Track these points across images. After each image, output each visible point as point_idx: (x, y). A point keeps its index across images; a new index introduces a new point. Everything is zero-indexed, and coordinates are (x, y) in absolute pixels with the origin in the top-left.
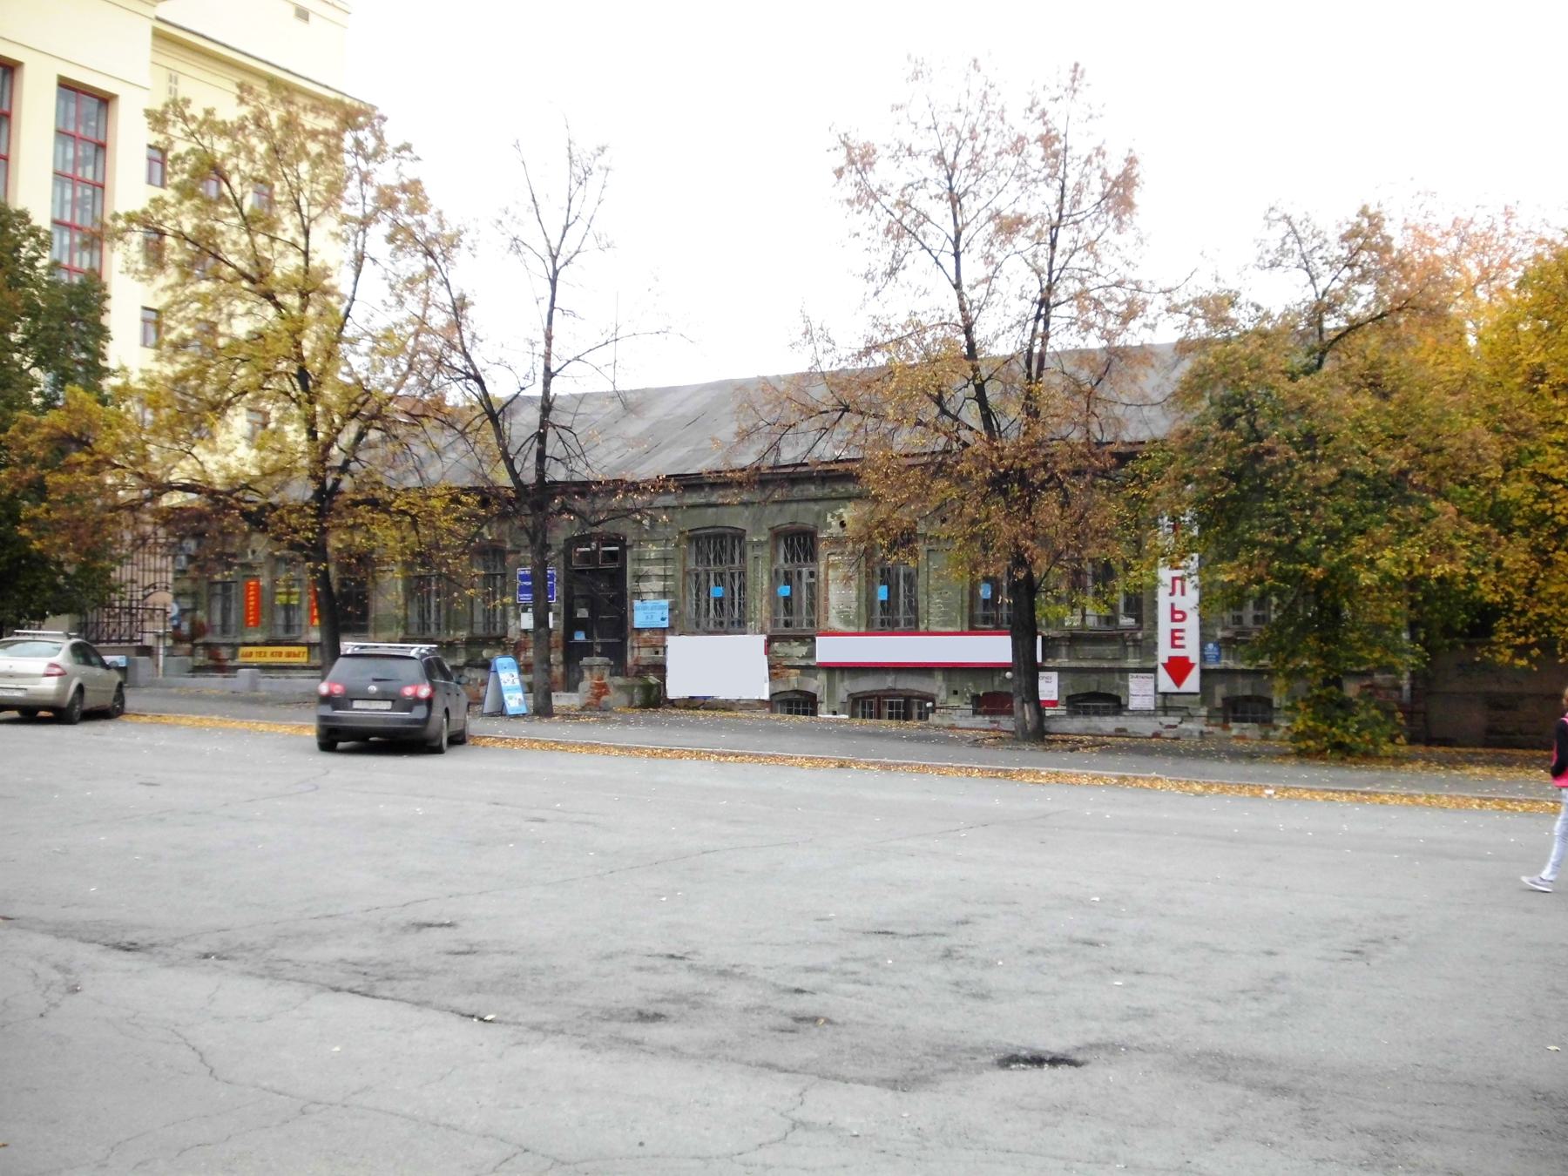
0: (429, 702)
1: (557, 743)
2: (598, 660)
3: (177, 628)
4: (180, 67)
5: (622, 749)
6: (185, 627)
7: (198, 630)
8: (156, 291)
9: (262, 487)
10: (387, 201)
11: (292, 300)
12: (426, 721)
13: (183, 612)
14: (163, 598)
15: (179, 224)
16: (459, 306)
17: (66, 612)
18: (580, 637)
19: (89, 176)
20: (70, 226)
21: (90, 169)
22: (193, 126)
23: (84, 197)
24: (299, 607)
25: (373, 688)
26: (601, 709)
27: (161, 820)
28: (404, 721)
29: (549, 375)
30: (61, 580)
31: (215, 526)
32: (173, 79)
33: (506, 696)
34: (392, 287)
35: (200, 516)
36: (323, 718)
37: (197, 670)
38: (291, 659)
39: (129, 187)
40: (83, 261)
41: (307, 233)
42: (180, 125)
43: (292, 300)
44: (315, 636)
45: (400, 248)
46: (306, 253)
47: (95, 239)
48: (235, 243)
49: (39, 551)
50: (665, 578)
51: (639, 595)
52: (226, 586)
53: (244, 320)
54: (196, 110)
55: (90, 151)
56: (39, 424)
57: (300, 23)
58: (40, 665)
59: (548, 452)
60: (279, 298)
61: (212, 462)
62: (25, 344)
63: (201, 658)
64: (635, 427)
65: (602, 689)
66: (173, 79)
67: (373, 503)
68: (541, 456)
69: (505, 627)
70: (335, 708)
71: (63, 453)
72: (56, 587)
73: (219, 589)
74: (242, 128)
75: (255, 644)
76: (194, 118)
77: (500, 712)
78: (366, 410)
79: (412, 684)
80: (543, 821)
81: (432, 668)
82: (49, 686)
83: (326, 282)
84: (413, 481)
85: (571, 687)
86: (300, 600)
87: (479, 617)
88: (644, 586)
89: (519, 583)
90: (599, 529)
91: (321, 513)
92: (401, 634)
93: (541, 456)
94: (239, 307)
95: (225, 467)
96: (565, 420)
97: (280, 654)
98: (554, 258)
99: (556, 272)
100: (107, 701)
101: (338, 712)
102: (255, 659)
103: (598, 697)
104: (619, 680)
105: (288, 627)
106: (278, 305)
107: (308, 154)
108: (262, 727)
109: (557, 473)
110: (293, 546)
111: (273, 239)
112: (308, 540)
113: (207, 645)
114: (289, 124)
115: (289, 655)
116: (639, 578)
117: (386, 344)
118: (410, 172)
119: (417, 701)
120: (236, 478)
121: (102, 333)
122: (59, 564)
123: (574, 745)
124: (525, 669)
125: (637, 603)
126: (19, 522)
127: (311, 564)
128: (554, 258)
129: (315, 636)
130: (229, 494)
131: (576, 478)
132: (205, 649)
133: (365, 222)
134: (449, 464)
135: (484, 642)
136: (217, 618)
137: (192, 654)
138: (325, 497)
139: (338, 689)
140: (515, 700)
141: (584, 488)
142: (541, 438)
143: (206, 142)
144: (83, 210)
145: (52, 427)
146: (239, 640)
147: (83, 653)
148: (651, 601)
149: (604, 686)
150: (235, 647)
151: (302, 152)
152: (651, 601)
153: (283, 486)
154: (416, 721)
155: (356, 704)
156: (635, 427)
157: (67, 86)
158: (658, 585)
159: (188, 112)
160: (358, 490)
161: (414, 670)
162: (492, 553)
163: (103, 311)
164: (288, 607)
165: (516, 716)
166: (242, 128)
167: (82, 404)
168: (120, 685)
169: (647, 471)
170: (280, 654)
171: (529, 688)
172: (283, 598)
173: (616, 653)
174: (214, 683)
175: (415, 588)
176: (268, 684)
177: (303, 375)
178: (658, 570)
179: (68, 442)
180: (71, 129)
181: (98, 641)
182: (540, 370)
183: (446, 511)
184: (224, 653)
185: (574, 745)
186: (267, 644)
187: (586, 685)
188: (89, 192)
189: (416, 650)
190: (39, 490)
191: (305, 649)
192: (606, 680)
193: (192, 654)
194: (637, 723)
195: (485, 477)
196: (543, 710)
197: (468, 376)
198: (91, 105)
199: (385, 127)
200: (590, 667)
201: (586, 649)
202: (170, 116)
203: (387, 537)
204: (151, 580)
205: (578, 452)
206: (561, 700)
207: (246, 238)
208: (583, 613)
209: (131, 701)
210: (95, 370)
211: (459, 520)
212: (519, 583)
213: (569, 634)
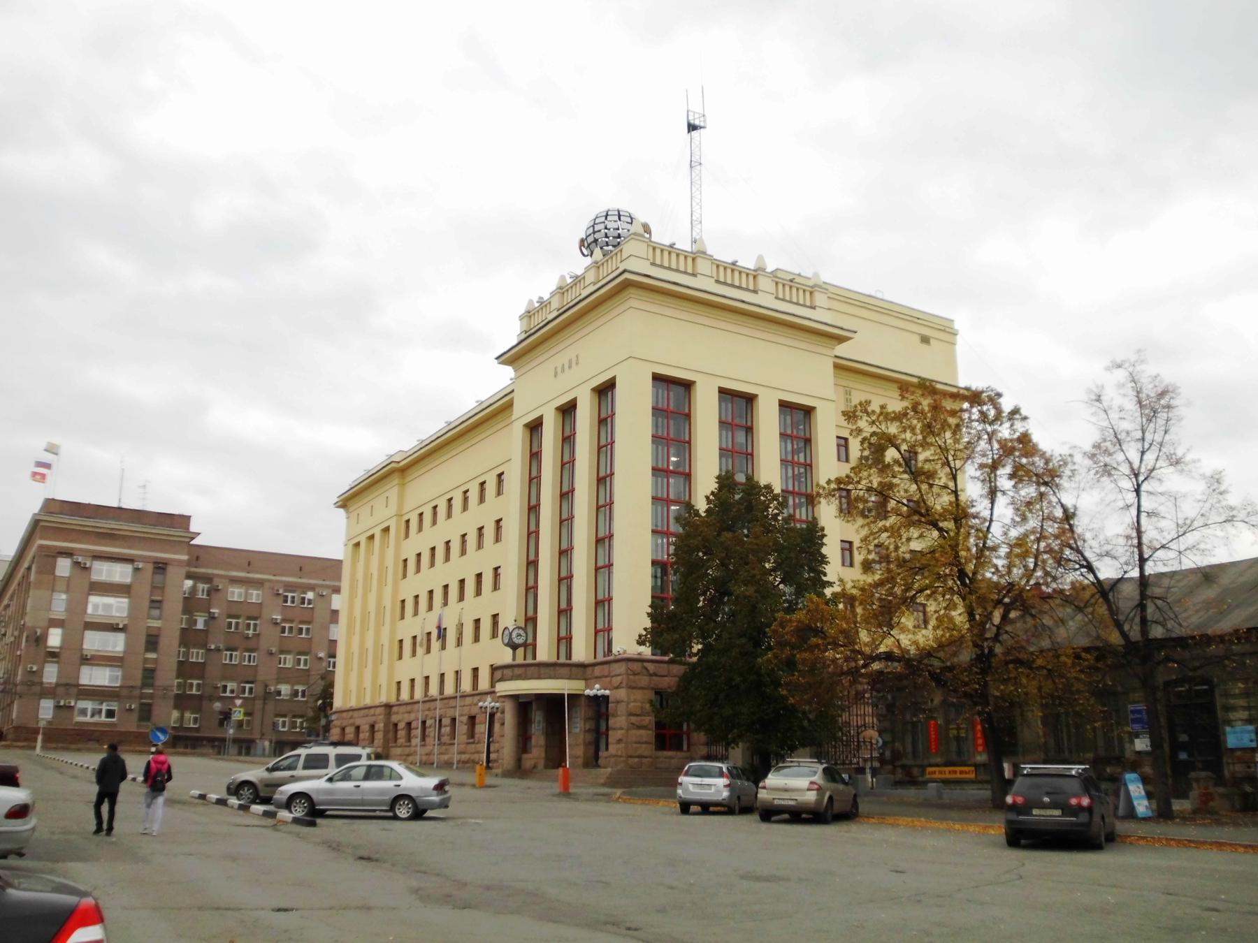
0: (1089, 809)
1: (1190, 841)
2: (1203, 774)
3: (882, 754)
4: (851, 384)
5: (1246, 847)
6: (888, 754)
7: (896, 756)
8: (854, 531)
9: (941, 654)
10: (1007, 449)
11: (948, 525)
12: (1088, 825)
13: (885, 743)
14: (872, 734)
15: (871, 482)
16: (1068, 516)
17: (810, 745)
18: (1183, 756)
19: (802, 460)
20: (793, 493)
21: (802, 455)
22: (874, 418)
23: (800, 473)
24: (967, 738)
25: (1046, 799)
26: (1209, 813)
27: (919, 901)
28: (1072, 823)
29: (1142, 561)
30: (805, 723)
31: (906, 681)
32: (848, 393)
33: (1135, 803)
34: (1018, 509)
35: (899, 677)
36: (1009, 823)
37: (898, 784)
38: (963, 776)
39: (828, 467)
40: (802, 514)
41: (954, 478)
42: (865, 418)
43: (948, 525)
44: (981, 758)
45: (1021, 481)
46: (955, 492)
47: (811, 500)
48: (906, 491)
49: (793, 705)
50: (1248, 708)
51: (1229, 722)
52: (914, 725)
53: (919, 541)
54: (875, 406)
55: (802, 444)
56: (790, 620)
57: (924, 346)
58: (803, 783)
59: (1149, 618)
60: (941, 525)
61: (905, 640)
62: (774, 569)
63: (899, 775)
64: (1210, 593)
65: (1207, 798)
66: (848, 393)
67: (1019, 662)
68: (1144, 621)
69: (1122, 750)
70: (1020, 813)
71: (805, 640)
72: (803, 728)
73: (909, 727)
74: (905, 414)
75: (937, 765)
76: (873, 412)
77: (1131, 814)
78: (1019, 599)
79: (1075, 796)
80: (1217, 910)
81: (1088, 784)
82: (811, 797)
83: (973, 510)
84: (1046, 644)
85: (1183, 795)
86: (967, 733)
87: (1101, 743)
88: (1232, 716)
89: (1131, 716)
90: (1199, 672)
91: (984, 672)
92: (1042, 756)
93: (1144, 621)
94: (914, 532)
95: (915, 643)
96: (1157, 591)
97: (955, 772)
98: (1136, 476)
99: (1139, 486)
100: (848, 807)
101: (1021, 817)
102: (937, 776)
103: (1206, 802)
104: (1221, 790)
105: (959, 753)
106: (940, 530)
107: (950, 426)
108: (957, 826)
109: (1157, 632)
110: (966, 695)
111: (931, 486)
112: (976, 690)
113: (903, 767)
114: (935, 408)
115: (961, 772)
116: (1228, 709)
117: (1019, 547)
118: (1020, 427)
119: (1080, 808)
120: (924, 649)
121: (823, 560)
122: (804, 713)
123: (1204, 843)
124: (1145, 780)
125: (1228, 729)
126: (779, 685)
127: (979, 708)
128: (1136, 476)
129: (981, 758)
130: (920, 662)
131: (1174, 635)
132: (902, 770)
133: (994, 466)
134: (1071, 630)
135: (1108, 761)
136: (909, 748)
137: (893, 772)
138: (984, 660)
139: (1020, 800)
140: (1142, 807)
141: (1181, 642)
142: (1142, 606)
143: (883, 427)
144: (800, 482)
145: (799, 621)
146: (926, 762)
147: (830, 774)
148: (1239, 727)
149: (1211, 794)
150: (923, 768)
151: (945, 426)
152: (1239, 727)
153: (955, 654)
154: (1082, 824)
155: (1035, 812)
156: (1210, 593)
157: (784, 406)
158: (1244, 714)
159: (870, 409)
160: (1005, 654)
161: (1075, 786)
162: (1103, 694)
163: (823, 544)
164: (958, 739)
165: (1144, 819)
166: (905, 414)
167: (817, 605)
168: (855, 796)
169: (1225, 625)
170: (955, 772)
171: (1149, 796)
172: (955, 732)
173: (1215, 767)
174: (911, 793)
175: (1052, 722)
176: (950, 794)
177: (962, 574)
178: (1242, 702)
179: (807, 632)
180: (789, 432)
181: (836, 764)
182: (1137, 557)
183: (1074, 665)
184: (916, 772)
185: (1204, 843)
186: (946, 765)
187: (1194, 794)
188: (802, 470)
189: (1075, 769)
190: (790, 664)
191: (972, 768)
192: (1211, 790)
193: (893, 772)
194: (1246, 825)
195: (1098, 637)
196: (1164, 814)
197: (1082, 566)
198: (800, 415)
199: (1001, 400)
200: (1197, 780)
201: (1189, 766)
202: (858, 413)
203: (1030, 685)
204: (864, 722)
205: (1172, 616)
206: (1178, 805)
207: (914, 487)
208: (1184, 738)
209: (863, 807)
210: (819, 583)
211: (1081, 671)
212: (1131, 716)
213: (1174, 754)
